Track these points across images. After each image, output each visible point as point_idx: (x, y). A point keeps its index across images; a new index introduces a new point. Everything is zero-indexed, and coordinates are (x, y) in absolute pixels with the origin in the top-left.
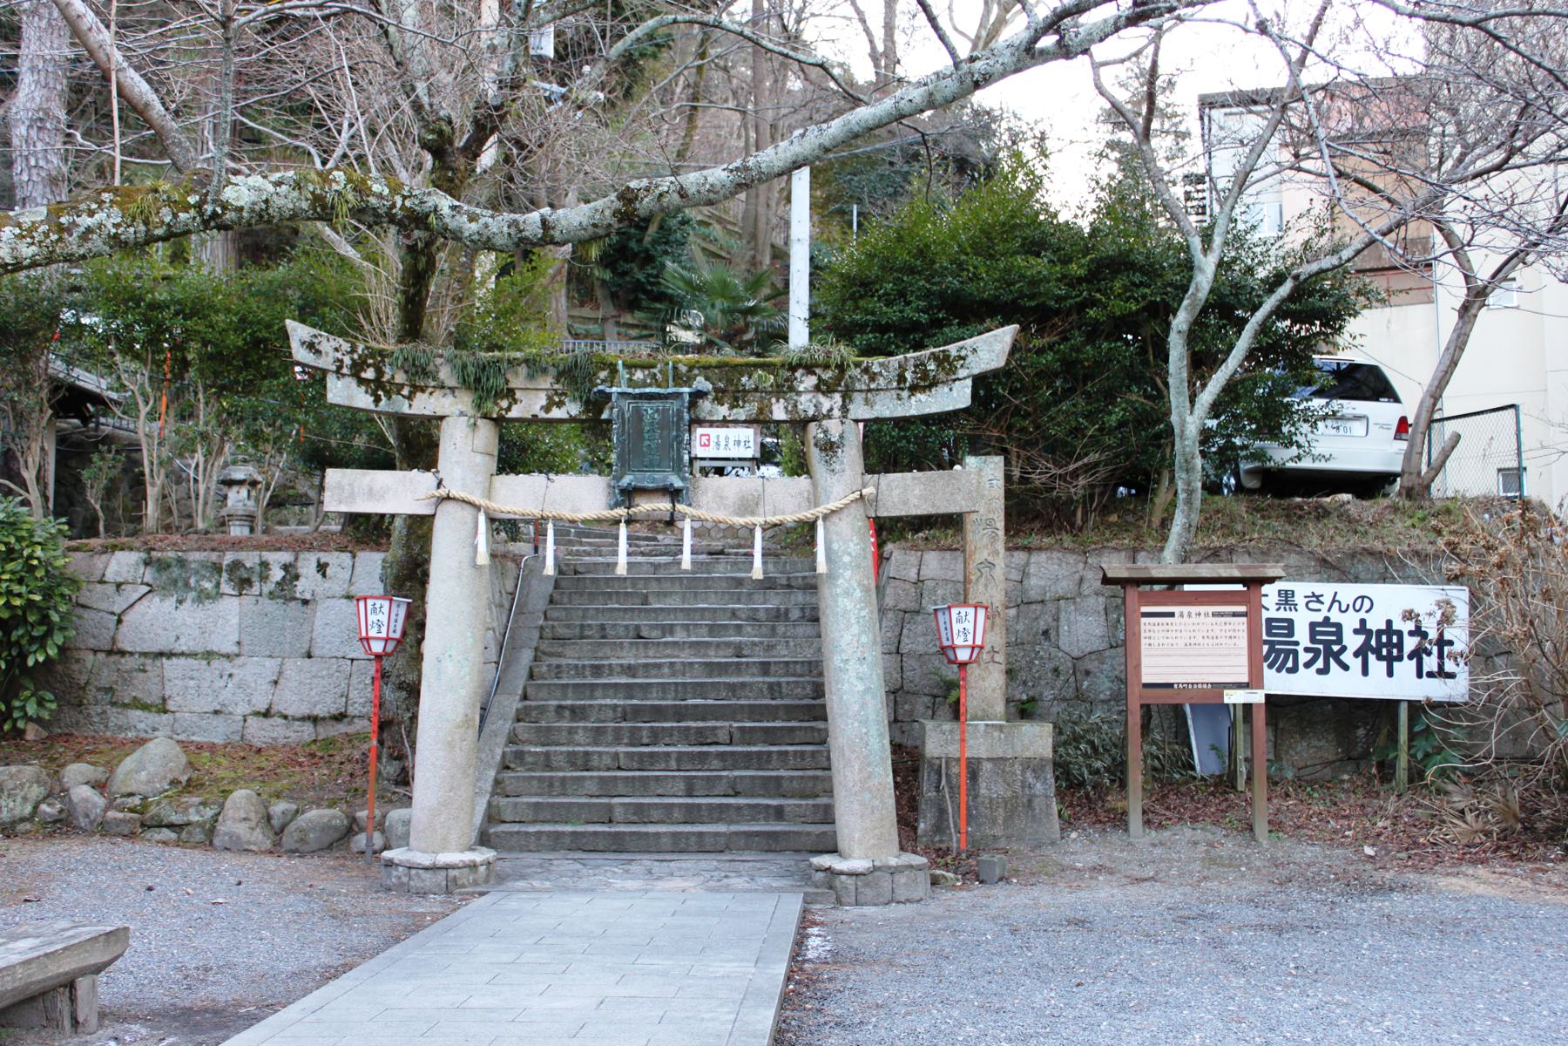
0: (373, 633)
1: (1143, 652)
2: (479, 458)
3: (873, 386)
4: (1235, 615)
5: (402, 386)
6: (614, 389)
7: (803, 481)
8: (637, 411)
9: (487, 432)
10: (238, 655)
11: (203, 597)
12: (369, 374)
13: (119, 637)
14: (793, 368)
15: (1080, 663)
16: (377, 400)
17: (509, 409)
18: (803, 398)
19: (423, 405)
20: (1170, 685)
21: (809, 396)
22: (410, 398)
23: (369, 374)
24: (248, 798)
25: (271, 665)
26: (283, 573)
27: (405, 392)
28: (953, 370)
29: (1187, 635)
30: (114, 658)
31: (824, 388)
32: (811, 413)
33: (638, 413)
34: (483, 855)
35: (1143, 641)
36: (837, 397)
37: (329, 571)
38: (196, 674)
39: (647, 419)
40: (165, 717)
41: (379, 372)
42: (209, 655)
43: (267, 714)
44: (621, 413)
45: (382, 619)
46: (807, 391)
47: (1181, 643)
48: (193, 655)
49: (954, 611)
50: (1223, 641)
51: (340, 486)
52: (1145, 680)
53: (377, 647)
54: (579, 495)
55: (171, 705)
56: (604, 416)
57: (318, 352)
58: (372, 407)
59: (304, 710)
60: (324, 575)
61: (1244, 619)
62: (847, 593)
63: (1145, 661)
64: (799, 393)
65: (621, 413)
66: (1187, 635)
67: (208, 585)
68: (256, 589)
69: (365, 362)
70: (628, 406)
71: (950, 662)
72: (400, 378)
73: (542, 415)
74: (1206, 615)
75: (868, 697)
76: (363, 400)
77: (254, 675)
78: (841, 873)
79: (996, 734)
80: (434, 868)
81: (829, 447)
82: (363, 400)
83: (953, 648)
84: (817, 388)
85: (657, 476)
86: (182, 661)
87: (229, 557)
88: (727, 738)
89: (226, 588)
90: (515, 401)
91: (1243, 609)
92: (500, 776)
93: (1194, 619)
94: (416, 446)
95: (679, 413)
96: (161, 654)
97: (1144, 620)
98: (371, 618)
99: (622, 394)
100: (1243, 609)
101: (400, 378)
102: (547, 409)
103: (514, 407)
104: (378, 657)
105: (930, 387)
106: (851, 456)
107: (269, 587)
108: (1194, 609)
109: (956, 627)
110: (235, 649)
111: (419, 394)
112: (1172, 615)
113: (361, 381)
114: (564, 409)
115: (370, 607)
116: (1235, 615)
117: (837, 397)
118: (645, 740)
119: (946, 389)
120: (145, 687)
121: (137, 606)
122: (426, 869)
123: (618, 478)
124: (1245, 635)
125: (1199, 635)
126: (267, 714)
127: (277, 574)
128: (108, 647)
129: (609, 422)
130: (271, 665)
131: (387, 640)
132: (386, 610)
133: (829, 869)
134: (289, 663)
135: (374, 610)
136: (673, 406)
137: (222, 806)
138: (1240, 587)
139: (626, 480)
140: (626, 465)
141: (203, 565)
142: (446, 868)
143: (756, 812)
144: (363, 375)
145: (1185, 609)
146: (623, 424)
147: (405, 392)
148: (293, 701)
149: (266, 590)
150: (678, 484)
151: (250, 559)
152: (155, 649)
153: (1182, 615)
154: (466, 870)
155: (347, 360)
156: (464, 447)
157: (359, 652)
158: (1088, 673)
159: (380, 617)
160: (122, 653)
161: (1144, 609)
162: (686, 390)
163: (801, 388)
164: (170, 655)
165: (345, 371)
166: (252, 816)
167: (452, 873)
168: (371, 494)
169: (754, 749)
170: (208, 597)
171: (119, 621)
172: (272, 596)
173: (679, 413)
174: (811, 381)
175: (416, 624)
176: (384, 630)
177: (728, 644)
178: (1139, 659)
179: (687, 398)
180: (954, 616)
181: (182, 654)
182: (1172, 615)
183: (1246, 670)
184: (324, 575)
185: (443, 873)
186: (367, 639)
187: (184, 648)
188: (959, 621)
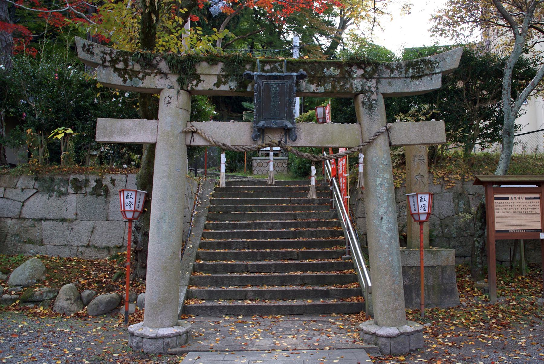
0: (127, 208)
1: (496, 216)
2: (180, 111)
3: (392, 76)
4: (535, 198)
5: (139, 72)
6: (255, 73)
7: (355, 126)
8: (267, 86)
9: (184, 97)
10: (76, 220)
11: (61, 194)
12: (121, 66)
13: (23, 212)
14: (351, 66)
15: (443, 221)
16: (125, 81)
17: (197, 85)
18: (355, 82)
19: (152, 82)
20: (507, 231)
21: (359, 80)
22: (142, 79)
23: (121, 66)
24: (71, 289)
25: (90, 224)
26: (96, 184)
27: (140, 76)
28: (433, 68)
29: (515, 207)
30: (20, 221)
31: (367, 77)
32: (360, 88)
33: (268, 87)
34: (185, 326)
35: (496, 211)
36: (374, 81)
37: (116, 182)
38: (57, 228)
39: (273, 91)
40: (42, 247)
41: (126, 65)
42: (63, 220)
43: (88, 246)
44: (259, 85)
45: (131, 201)
46: (358, 78)
47: (512, 211)
48: (56, 220)
49: (419, 196)
50: (530, 210)
51: (105, 128)
52: (497, 228)
53: (130, 215)
54: (234, 133)
55: (45, 242)
56: (249, 89)
57: (92, 53)
58: (122, 84)
59: (104, 245)
60: (114, 185)
61: (539, 200)
62: (503, 158)
63: (496, 220)
64: (353, 79)
65: (259, 85)
66: (515, 207)
67: (63, 189)
68: (84, 191)
69: (118, 59)
70: (262, 83)
71: (415, 221)
72: (137, 67)
73: (215, 88)
74: (523, 198)
75: (393, 241)
76: (116, 80)
77: (83, 227)
78: (383, 336)
79: (430, 255)
80: (156, 338)
81: (371, 107)
82: (116, 80)
83: (419, 214)
84: (363, 76)
85: (278, 121)
86: (51, 222)
87: (72, 177)
88: (296, 256)
89: (71, 190)
90: (200, 81)
91: (538, 196)
92: (193, 277)
93: (517, 200)
94: (145, 106)
95: (291, 87)
96: (41, 219)
97: (495, 201)
98: (127, 200)
99: (258, 76)
100: (538, 196)
101: (137, 67)
102: (218, 85)
103: (200, 84)
104: (130, 221)
105: (420, 77)
106: (381, 110)
107: (89, 190)
108: (517, 196)
109: (420, 204)
110: (74, 217)
111: (147, 77)
112: (507, 198)
113: (116, 70)
114: (227, 85)
115: (125, 195)
116: (535, 198)
117: (374, 81)
118: (258, 258)
119: (429, 79)
120: (35, 233)
121: (31, 199)
122: (152, 338)
123: (257, 122)
124: (539, 207)
125: (519, 208)
126: (88, 246)
127: (93, 184)
128: (18, 217)
129: (252, 93)
130: (90, 224)
131: (134, 211)
132: (134, 196)
133: (375, 334)
134: (98, 224)
135: (128, 197)
136: (287, 83)
137: (58, 293)
138: (535, 186)
139: (261, 124)
140: (260, 115)
141: (61, 180)
142: (164, 337)
143: (316, 295)
144: (117, 66)
145: (513, 196)
146: (260, 93)
147: (140, 76)
148: (100, 240)
149: (88, 191)
150: (290, 125)
151: (81, 178)
152: (39, 216)
153: (512, 199)
154: (175, 338)
155: (108, 58)
156: (172, 105)
157: (121, 218)
158: (447, 226)
159: (131, 200)
160: (24, 219)
161: (496, 196)
162: (295, 74)
163: (355, 76)
164: (46, 220)
165: (107, 64)
166: (72, 297)
167: (167, 340)
168: (122, 132)
169: (240, 240)
170: (63, 194)
171: (23, 205)
172: (92, 194)
173: (291, 87)
174: (361, 72)
175: (147, 203)
176: (133, 206)
177: (290, 214)
178: (494, 219)
179: (295, 78)
180: (419, 198)
181: (51, 219)
182: (507, 198)
183: (540, 223)
184: (114, 185)
185: (161, 340)
186: (124, 212)
187: (52, 217)
188: (422, 201)
